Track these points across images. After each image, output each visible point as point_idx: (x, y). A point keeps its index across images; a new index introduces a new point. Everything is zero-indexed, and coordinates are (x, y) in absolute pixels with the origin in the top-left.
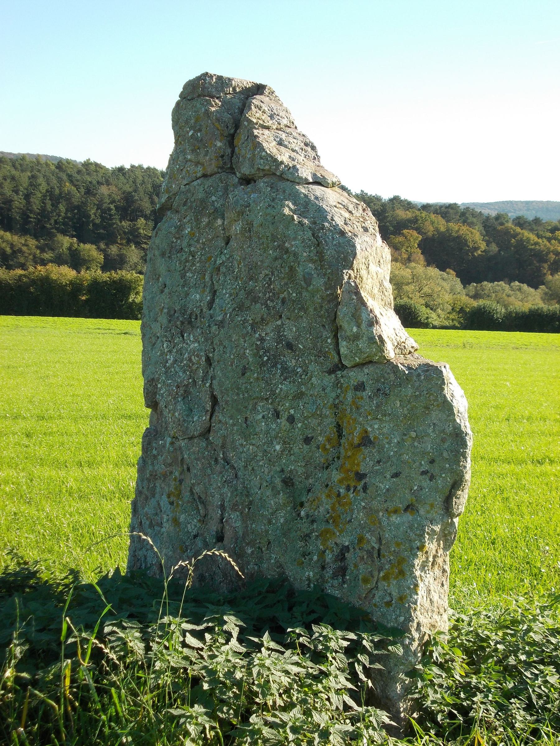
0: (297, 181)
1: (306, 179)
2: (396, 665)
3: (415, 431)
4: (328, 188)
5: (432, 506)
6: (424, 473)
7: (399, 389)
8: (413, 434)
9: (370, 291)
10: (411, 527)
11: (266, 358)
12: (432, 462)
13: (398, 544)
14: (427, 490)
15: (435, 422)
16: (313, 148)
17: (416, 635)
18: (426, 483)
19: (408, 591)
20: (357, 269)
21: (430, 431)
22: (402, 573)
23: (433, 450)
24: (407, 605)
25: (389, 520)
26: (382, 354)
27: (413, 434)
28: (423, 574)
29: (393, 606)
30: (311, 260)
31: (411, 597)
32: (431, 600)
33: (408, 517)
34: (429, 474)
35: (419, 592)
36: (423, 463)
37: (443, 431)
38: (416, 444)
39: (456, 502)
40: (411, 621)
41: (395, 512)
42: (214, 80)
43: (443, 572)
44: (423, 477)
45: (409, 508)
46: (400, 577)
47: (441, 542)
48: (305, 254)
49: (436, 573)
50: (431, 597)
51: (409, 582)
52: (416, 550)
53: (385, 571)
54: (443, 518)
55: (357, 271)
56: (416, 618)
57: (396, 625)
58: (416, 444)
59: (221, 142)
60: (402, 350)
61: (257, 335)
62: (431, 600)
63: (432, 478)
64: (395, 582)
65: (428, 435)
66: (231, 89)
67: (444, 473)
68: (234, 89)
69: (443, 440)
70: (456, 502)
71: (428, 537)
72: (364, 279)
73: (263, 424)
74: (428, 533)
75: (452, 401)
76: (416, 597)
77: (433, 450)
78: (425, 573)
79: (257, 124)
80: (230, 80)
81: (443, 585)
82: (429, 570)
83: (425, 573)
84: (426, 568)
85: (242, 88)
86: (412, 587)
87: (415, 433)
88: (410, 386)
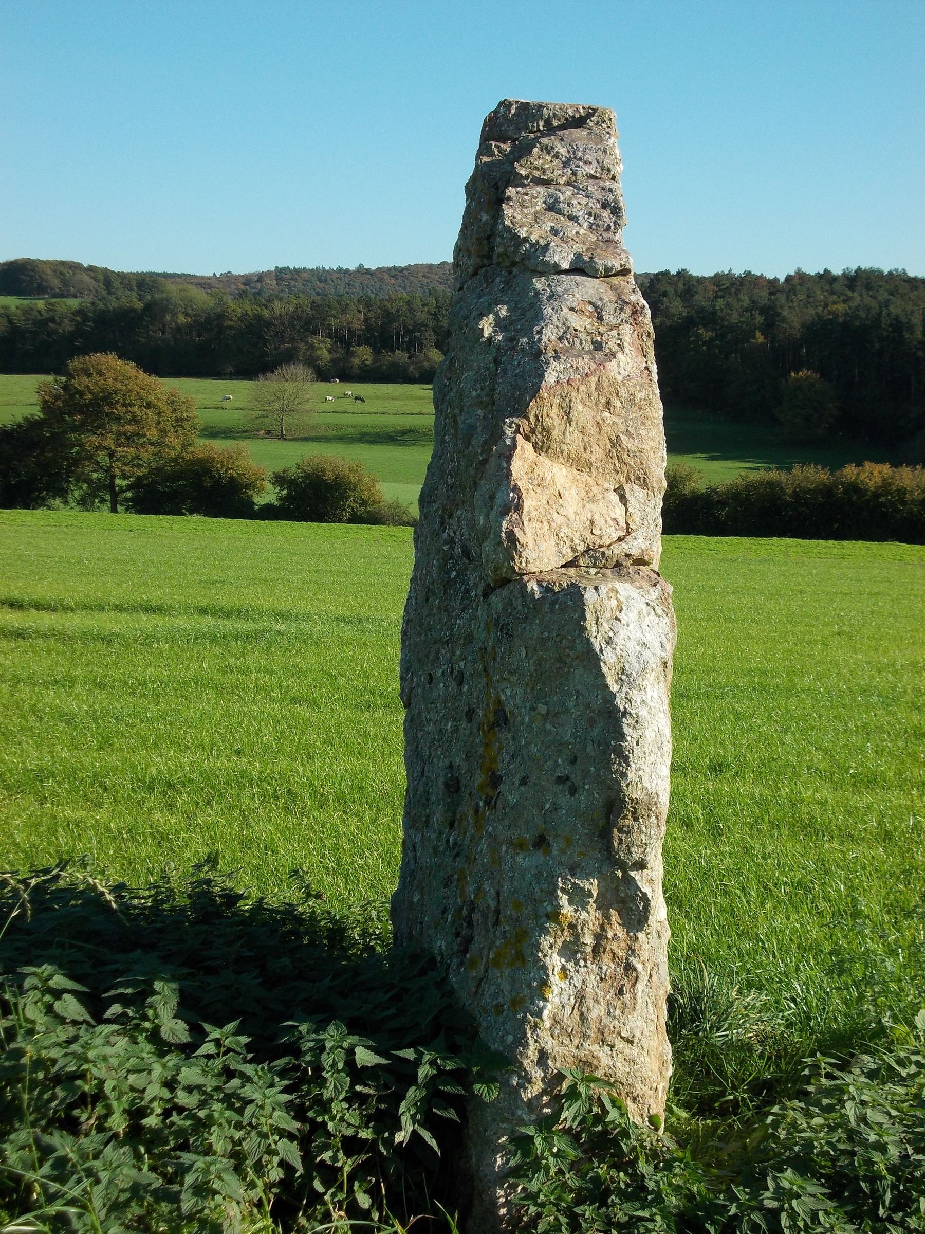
0: (540, 269)
1: (556, 265)
2: (494, 1120)
3: (546, 704)
4: (597, 278)
5: (569, 841)
6: (562, 780)
7: (524, 625)
8: (542, 709)
9: (573, 455)
10: (538, 876)
11: (454, 573)
12: (573, 761)
13: (518, 905)
14: (564, 812)
15: (579, 688)
16: (616, 211)
17: (537, 1074)
18: (564, 800)
19: (526, 991)
20: (536, 416)
21: (571, 704)
22: (520, 957)
23: (575, 739)
24: (520, 1016)
25: (515, 861)
26: (509, 564)
27: (542, 709)
28: (570, 966)
29: (504, 1014)
30: (481, 404)
31: (533, 1003)
32: (582, 1014)
33: (539, 858)
34: (569, 783)
35: (550, 997)
36: (560, 761)
37: (588, 706)
38: (548, 726)
39: (620, 840)
40: (521, 1045)
41: (521, 846)
42: (513, 111)
43: (626, 969)
44: (560, 787)
45: (541, 842)
46: (518, 964)
47: (612, 912)
48: (474, 393)
49: (604, 968)
50: (584, 1009)
51: (532, 975)
52: (544, 919)
53: (495, 949)
54: (600, 867)
55: (538, 420)
56: (536, 1041)
57: (501, 1048)
58: (548, 726)
59: (487, 213)
60: (596, 559)
61: (445, 535)
62: (582, 1014)
63: (573, 791)
64: (507, 971)
65: (567, 711)
66: (541, 123)
67: (588, 783)
68: (548, 122)
69: (592, 722)
70: (620, 840)
71: (565, 897)
72: (555, 433)
73: (442, 685)
74: (564, 891)
75: (601, 650)
76: (541, 1003)
77: (575, 739)
78: (577, 963)
79: (527, 177)
80: (540, 107)
81: (621, 992)
82: (585, 960)
83: (577, 963)
84: (579, 956)
85: (566, 119)
86: (535, 984)
87: (545, 707)
88: (537, 621)
